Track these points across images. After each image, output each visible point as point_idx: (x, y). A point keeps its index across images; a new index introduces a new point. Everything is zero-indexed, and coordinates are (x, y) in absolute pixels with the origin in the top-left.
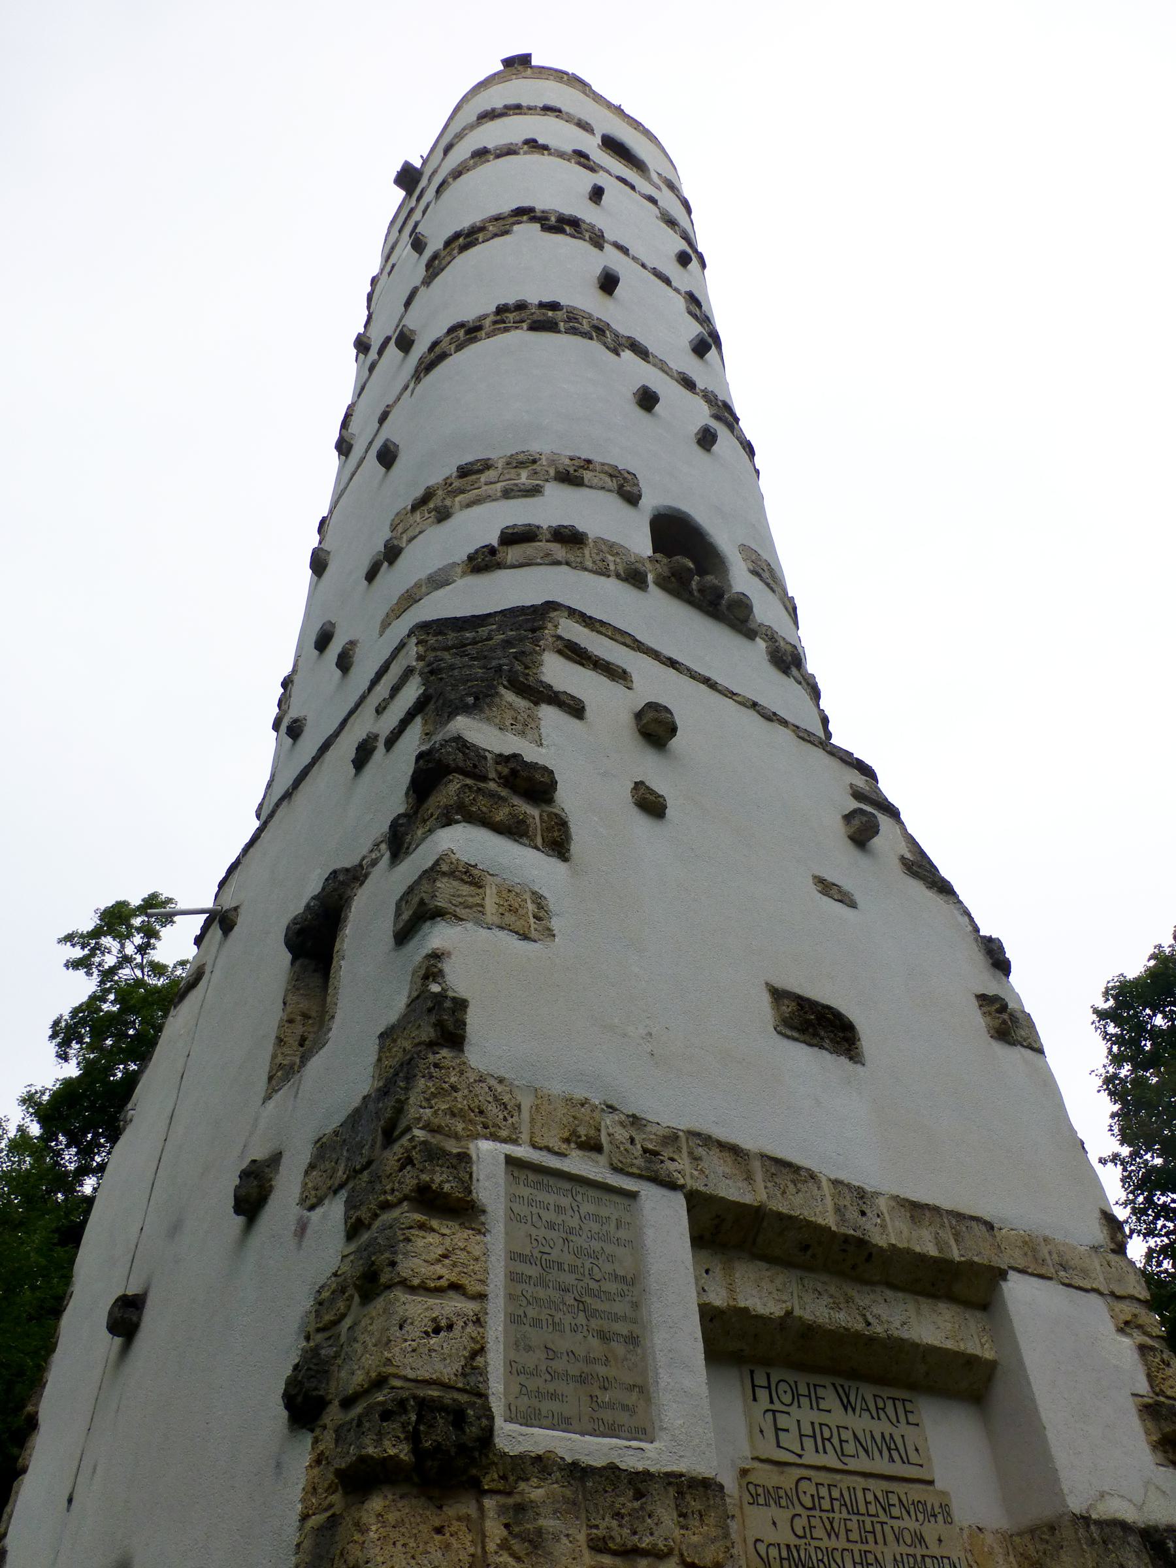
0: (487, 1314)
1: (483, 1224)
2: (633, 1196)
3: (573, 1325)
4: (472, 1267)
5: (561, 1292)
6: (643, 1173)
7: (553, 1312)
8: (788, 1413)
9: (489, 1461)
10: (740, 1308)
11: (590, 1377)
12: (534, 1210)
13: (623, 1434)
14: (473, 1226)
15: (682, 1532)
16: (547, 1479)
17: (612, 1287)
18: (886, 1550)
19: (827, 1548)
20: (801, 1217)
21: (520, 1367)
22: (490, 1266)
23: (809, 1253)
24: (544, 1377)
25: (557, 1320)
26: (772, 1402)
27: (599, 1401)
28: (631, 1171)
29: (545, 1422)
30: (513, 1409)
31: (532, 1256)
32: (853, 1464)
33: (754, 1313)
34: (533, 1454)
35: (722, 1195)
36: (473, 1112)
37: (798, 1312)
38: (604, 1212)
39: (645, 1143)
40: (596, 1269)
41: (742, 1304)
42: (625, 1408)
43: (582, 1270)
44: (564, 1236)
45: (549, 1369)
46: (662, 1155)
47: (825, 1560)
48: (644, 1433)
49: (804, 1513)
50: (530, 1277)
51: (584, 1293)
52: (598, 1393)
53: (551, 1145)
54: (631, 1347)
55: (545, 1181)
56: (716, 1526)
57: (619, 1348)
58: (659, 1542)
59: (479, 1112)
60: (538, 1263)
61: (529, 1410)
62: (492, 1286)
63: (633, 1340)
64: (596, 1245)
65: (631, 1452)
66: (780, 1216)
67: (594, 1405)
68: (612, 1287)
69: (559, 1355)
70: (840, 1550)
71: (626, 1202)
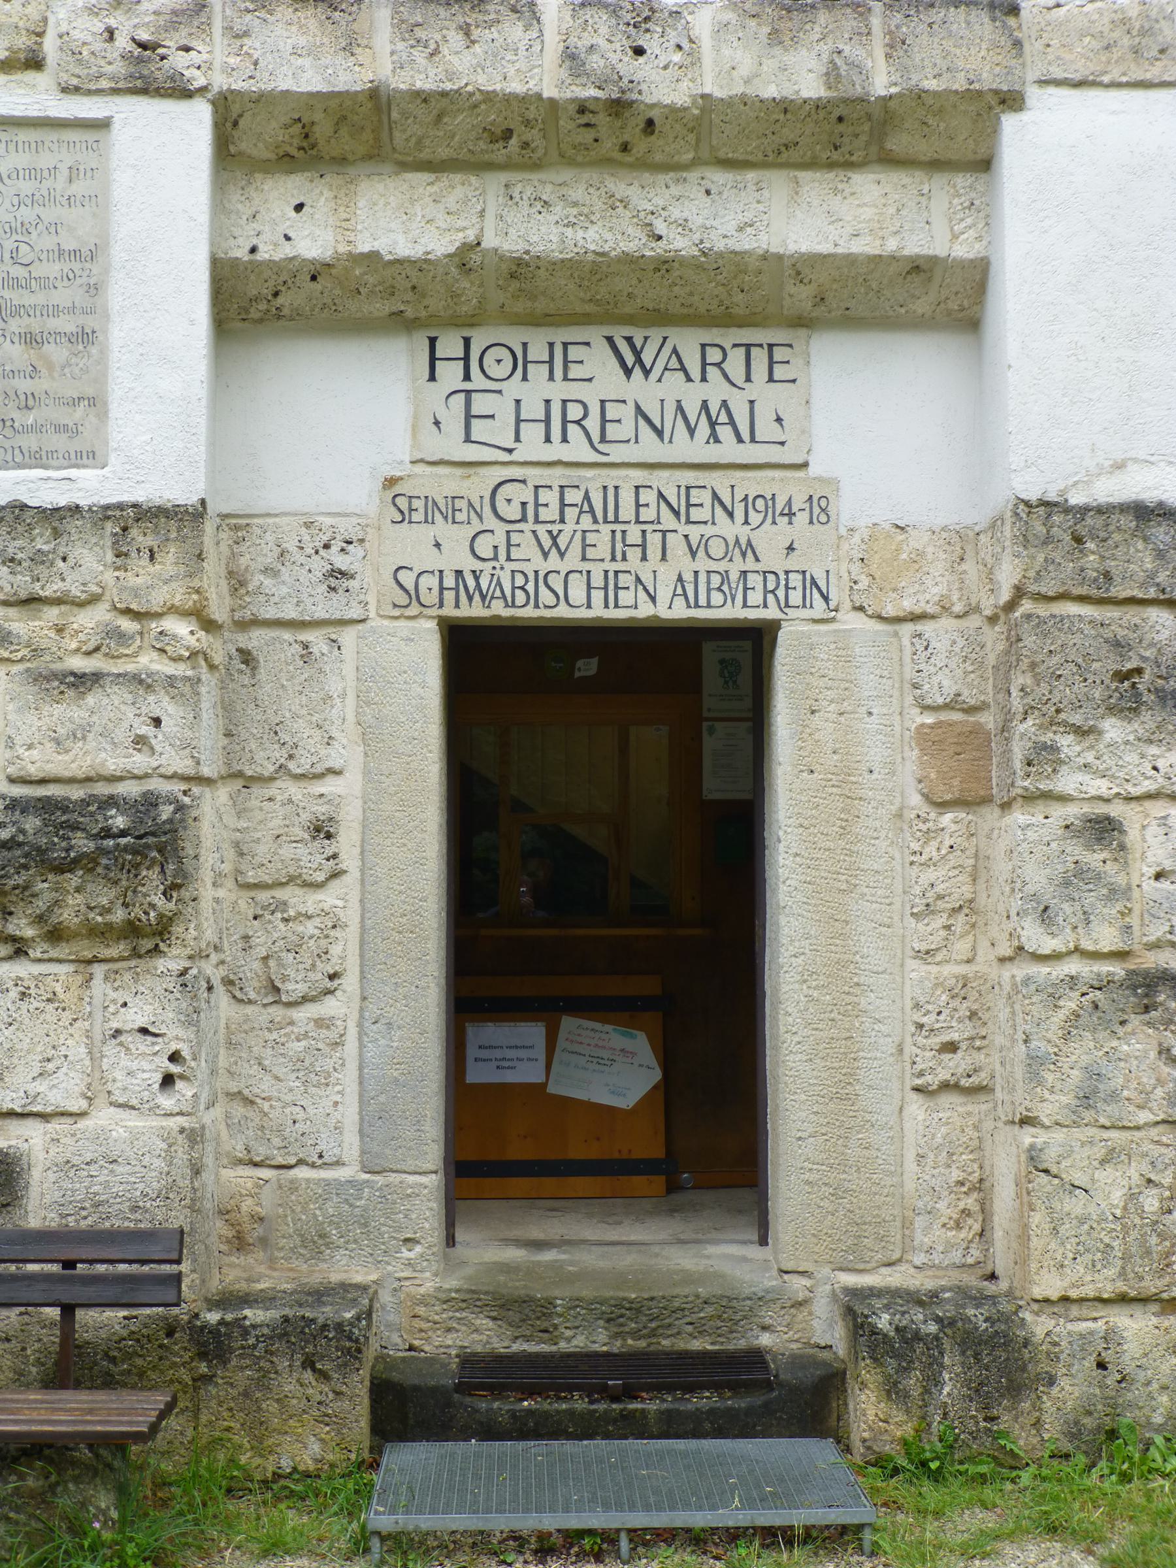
2: (102, 125)
6: (121, 85)
8: (500, 392)
10: (362, 254)
13: (54, 463)
15: (117, 574)
17: (52, 269)
18: (662, 569)
19: (536, 572)
20: (470, 88)
23: (514, 141)
26: (467, 377)
27: (16, 425)
32: (617, 454)
33: (389, 257)
35: (283, 86)
37: (490, 241)
38: (45, 160)
39: (140, 32)
40: (24, 248)
41: (364, 247)
42: (60, 428)
46: (164, 47)
47: (530, 588)
48: (91, 457)
49: (500, 529)
52: (16, 415)
54: (81, 347)
56: (176, 563)
57: (57, 352)
58: (73, 588)
63: (85, 338)
64: (27, 214)
65: (51, 484)
66: (423, 97)
67: (8, 432)
68: (52, 269)
70: (563, 574)
71: (90, 136)
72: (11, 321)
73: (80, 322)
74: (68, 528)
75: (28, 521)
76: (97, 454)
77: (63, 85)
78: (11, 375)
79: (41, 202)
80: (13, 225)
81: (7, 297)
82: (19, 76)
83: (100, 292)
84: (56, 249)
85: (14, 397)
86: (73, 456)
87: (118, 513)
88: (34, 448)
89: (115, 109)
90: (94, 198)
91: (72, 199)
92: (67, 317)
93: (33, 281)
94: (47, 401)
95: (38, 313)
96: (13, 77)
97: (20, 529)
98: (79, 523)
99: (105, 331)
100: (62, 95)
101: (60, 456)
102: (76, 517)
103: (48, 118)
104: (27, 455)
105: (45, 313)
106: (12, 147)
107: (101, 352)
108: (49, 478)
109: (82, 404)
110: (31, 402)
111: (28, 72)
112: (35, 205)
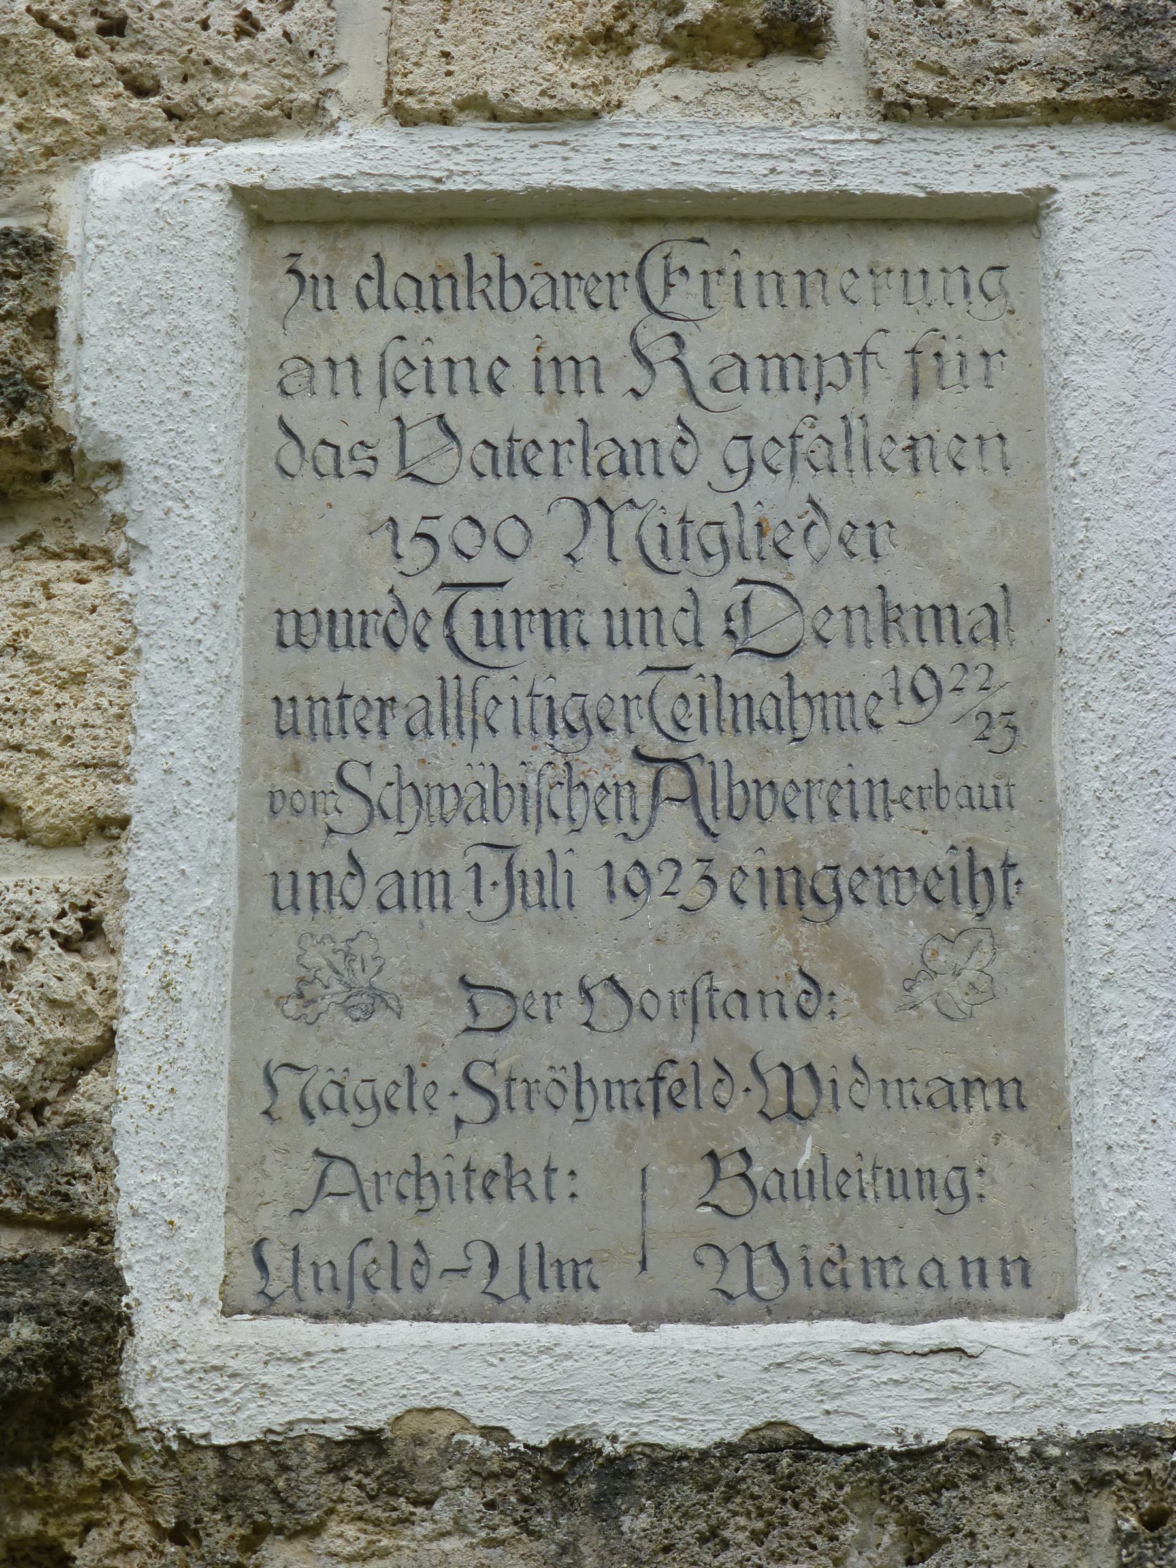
0: (125, 895)
1: (119, 521)
3: (622, 867)
4: (48, 717)
5: (562, 740)
6: (1075, 93)
7: (512, 829)
9: (84, 1481)
11: (709, 1076)
12: (418, 407)
13: (890, 1298)
14: (81, 539)
16: (407, 1520)
21: (318, 1082)
22: (143, 696)
24: (447, 1109)
25: (531, 858)
27: (757, 1171)
28: (1005, 97)
29: (444, 1293)
30: (275, 1256)
31: (400, 609)
34: (336, 1432)
36: (67, 34)
40: (767, 602)
43: (685, 626)
44: (586, 491)
45: (481, 1075)
50: (387, 703)
51: (693, 723)
52: (755, 1138)
53: (494, 89)
54: (966, 915)
55: (485, 263)
59: (103, 31)
60: (434, 634)
61: (364, 1255)
62: (144, 777)
65: (896, 1369)
67: (732, 1195)
69: (539, 1008)
72: (728, 830)
73: (961, 835)
74: (969, 1517)
75: (824, 1495)
76: (1038, 1267)
77: (892, 95)
78: (735, 1006)
79: (820, 460)
80: (732, 531)
81: (718, 758)
82: (741, 75)
83: (1024, 737)
84: (874, 605)
85: (750, 1080)
86: (953, 1274)
87: (1133, 1466)
88: (821, 1249)
89: (1059, 165)
90: (993, 445)
91: (924, 448)
92: (916, 819)
93: (800, 704)
94: (860, 1094)
95: (820, 807)
96: (724, 79)
97: (800, 1522)
98: (1005, 1501)
99: (1047, 864)
100: (885, 129)
101: (911, 1275)
102: (993, 1479)
103: (845, 196)
104: (796, 1272)
105: (842, 805)
106: (722, 290)
107: (1038, 930)
108: (887, 1349)
109: (977, 1105)
110: (804, 1096)
111: (772, 60)
112: (803, 466)
